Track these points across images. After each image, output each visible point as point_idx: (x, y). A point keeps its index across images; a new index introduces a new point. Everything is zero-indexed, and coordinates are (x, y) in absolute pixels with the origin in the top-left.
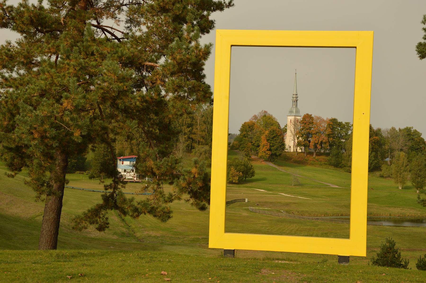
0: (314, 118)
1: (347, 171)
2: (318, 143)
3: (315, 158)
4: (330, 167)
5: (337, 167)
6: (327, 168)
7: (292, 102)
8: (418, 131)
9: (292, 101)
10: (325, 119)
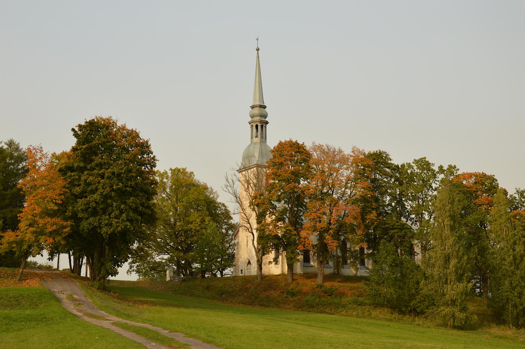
0: (315, 155)
1: (445, 325)
2: (327, 230)
3: (321, 286)
4: (375, 313)
5: (401, 312)
6: (364, 317)
7: (250, 129)
8: (474, 172)
9: (249, 126)
10: (347, 151)
